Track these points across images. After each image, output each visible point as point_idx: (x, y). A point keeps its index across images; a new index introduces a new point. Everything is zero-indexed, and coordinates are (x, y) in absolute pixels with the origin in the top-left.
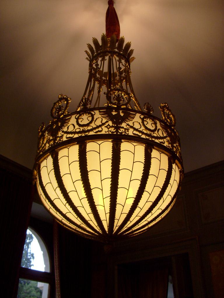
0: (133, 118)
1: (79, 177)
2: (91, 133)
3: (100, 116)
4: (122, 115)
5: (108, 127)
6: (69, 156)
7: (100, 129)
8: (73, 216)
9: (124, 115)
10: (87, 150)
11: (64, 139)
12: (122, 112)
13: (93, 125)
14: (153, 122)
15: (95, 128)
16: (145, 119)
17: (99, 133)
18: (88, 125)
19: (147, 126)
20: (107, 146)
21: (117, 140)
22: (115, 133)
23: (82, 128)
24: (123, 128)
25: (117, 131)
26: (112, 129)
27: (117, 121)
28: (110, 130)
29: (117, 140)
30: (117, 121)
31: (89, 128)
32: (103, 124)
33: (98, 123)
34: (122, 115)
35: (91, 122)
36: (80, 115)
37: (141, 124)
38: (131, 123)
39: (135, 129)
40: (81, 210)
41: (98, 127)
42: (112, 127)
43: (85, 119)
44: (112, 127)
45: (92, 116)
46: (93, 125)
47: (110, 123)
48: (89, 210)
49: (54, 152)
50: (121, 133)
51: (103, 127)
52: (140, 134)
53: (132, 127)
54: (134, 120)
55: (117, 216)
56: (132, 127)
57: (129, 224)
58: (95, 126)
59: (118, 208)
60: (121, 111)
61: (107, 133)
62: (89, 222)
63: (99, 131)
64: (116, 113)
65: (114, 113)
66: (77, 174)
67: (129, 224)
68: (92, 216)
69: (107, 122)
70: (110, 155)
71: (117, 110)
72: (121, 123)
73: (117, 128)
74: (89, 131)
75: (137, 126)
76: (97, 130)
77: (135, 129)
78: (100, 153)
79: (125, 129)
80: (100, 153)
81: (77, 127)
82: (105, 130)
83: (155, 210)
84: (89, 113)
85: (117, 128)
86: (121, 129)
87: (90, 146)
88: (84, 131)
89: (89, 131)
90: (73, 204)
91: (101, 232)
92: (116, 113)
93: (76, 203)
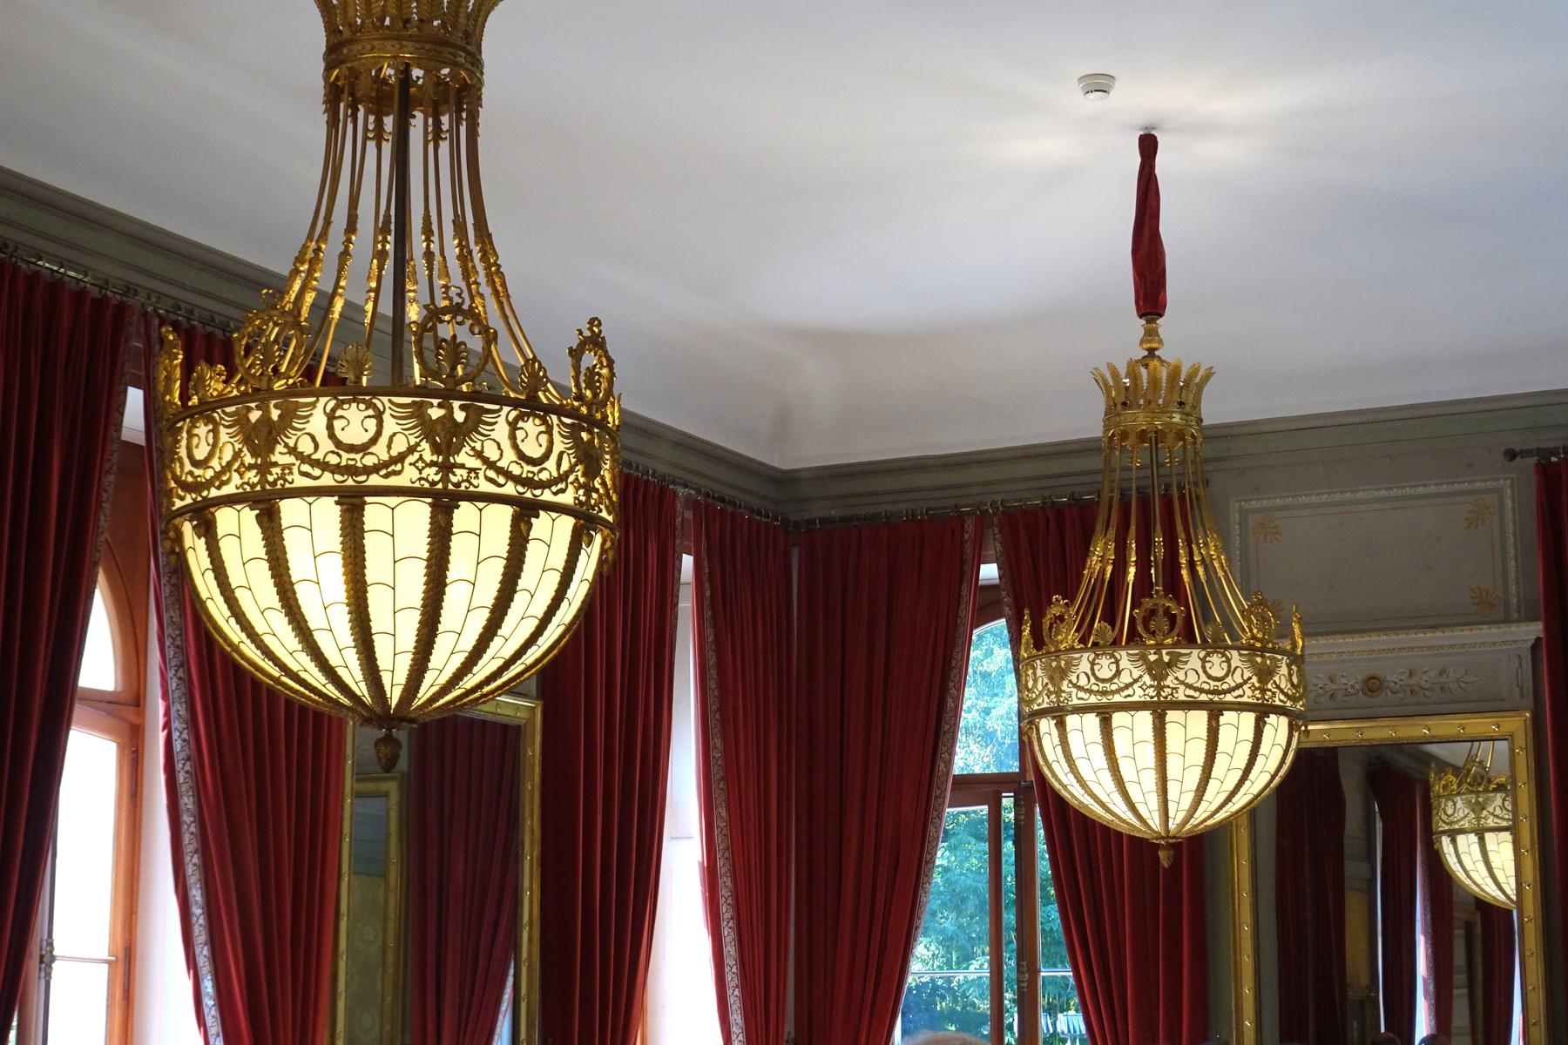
2: (1229, 698)
3: (398, 428)
4: (460, 416)
5: (420, 464)
7: (1130, 691)
8: (316, 677)
9: (466, 419)
11: (1182, 698)
12: (462, 408)
13: (380, 452)
14: (543, 428)
15: (1234, 689)
16: (520, 424)
18: (363, 449)
19: (522, 446)
22: (440, 486)
24: (462, 466)
25: (445, 480)
26: (431, 473)
27: (447, 439)
28: (424, 475)
29: (1262, 712)
30: (447, 439)
31: (1225, 687)
33: (1125, 678)
34: (460, 416)
35: (1227, 675)
36: (1208, 654)
37: (1200, 671)
38: (1181, 676)
39: (1190, 686)
42: (433, 464)
44: (433, 464)
45: (1228, 661)
47: (1147, 679)
49: (1059, 714)
50: (458, 485)
52: (1196, 694)
53: (1182, 683)
56: (1182, 683)
60: (456, 404)
61: (417, 485)
62: (303, 675)
64: (442, 412)
65: (1152, 658)
69: (411, 450)
71: (446, 396)
73: (447, 468)
74: (368, 471)
75: (1192, 679)
76: (1126, 693)
77: (1190, 686)
78: (1134, 729)
79: (471, 470)
81: (1203, 678)
82: (1138, 695)
84: (370, 405)
85: (447, 468)
86: (456, 471)
89: (368, 471)
90: (326, 661)
91: (368, 699)
92: (442, 412)
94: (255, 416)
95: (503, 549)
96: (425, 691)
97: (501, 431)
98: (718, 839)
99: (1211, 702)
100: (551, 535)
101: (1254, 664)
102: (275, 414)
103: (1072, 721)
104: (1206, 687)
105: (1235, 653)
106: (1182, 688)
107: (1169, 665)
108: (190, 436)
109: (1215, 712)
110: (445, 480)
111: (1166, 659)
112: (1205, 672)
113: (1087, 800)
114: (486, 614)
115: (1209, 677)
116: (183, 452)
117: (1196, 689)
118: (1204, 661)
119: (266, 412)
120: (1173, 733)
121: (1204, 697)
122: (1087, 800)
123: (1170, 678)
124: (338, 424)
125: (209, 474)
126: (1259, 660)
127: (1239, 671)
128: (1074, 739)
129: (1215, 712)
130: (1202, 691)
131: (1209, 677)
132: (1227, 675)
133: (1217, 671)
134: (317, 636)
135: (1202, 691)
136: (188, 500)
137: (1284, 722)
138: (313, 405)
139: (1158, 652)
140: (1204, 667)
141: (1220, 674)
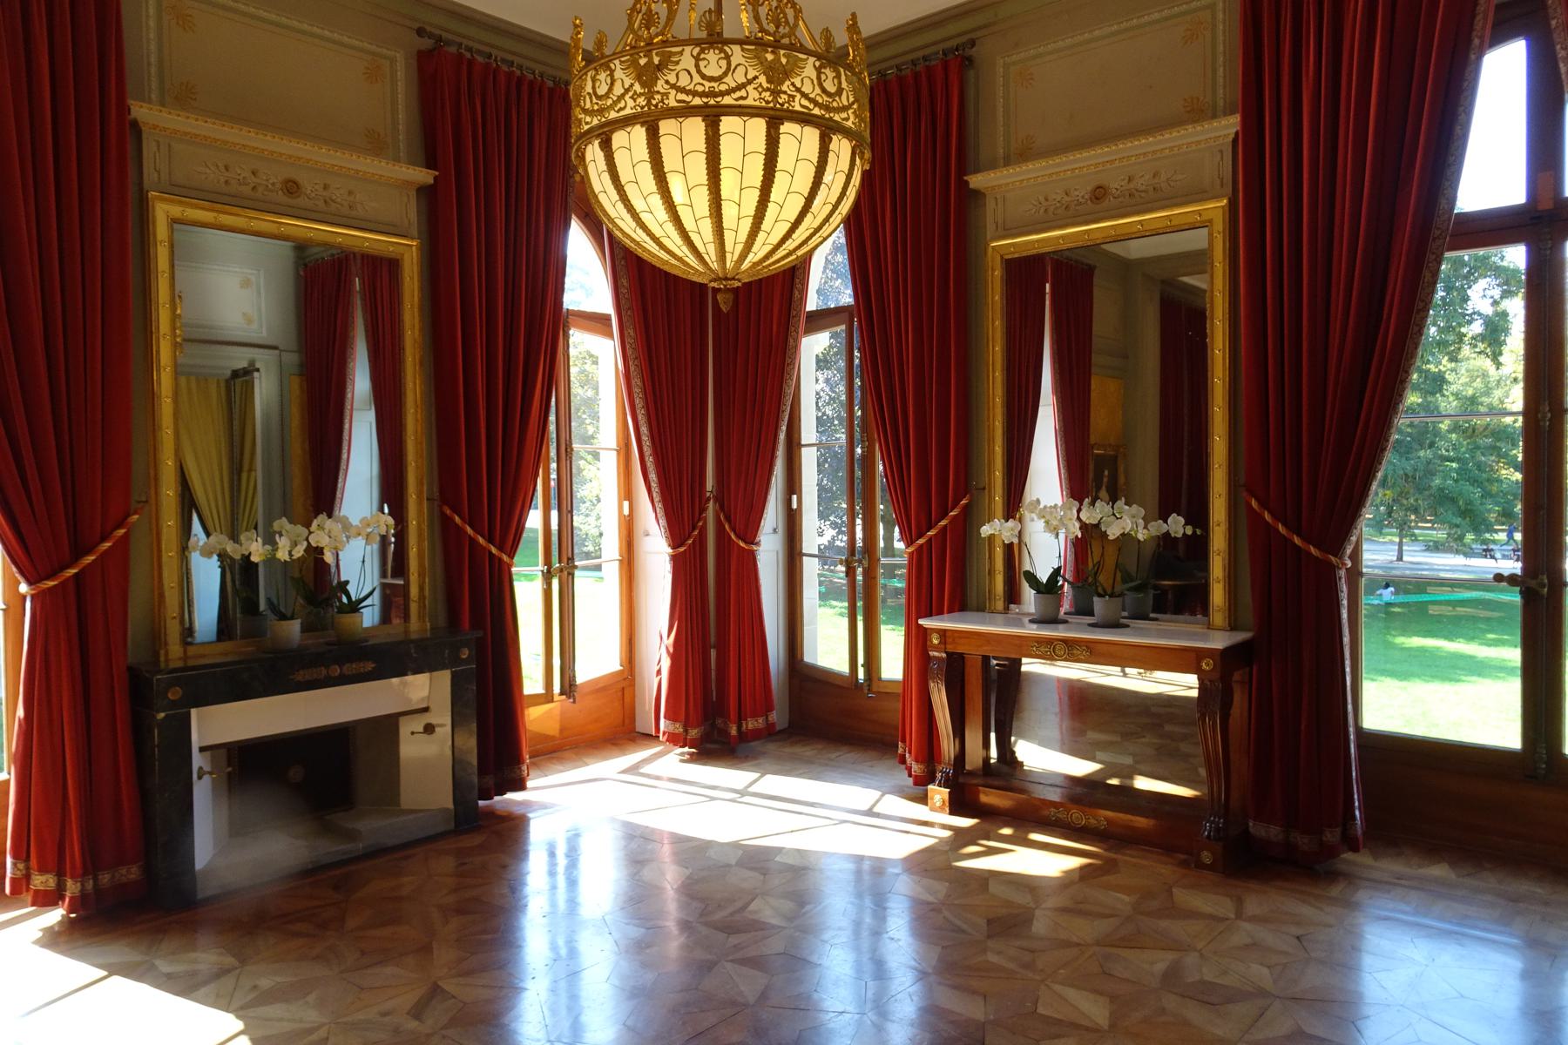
0: (677, 63)
1: (654, 188)
2: (727, 100)
3: (743, 61)
6: (631, 144)
7: (743, 93)
10: (661, 132)
11: (673, 103)
13: (730, 82)
15: (734, 90)
17: (741, 102)
18: (719, 79)
20: (639, 133)
21: (775, 119)
23: (707, 84)
25: (775, 101)
26: (766, 95)
27: (777, 75)
29: (775, 119)
31: (723, 87)
32: (749, 82)
35: (725, 74)
36: (702, 51)
40: (665, 241)
41: (740, 87)
43: (713, 64)
45: (728, 58)
46: (730, 82)
48: (679, 241)
51: (750, 88)
54: (678, 68)
55: (729, 247)
56: (673, 86)
57: (752, 258)
58: (733, 85)
59: (729, 237)
63: (742, 98)
66: (649, 183)
67: (752, 258)
68: (685, 249)
69: (756, 78)
70: (762, 146)
72: (782, 83)
73: (776, 93)
74: (722, 94)
75: (684, 81)
76: (738, 94)
79: (663, 94)
80: (742, 140)
81: (697, 78)
82: (752, 98)
83: (798, 232)
84: (722, 51)
85: (776, 93)
87: (728, 123)
88: (827, 108)
93: (689, 224)
94: (643, 61)
95: (762, 148)
96: (746, 265)
97: (687, 61)
98: (629, 352)
99: (706, 105)
100: (841, 148)
101: (762, 62)
102: (656, 60)
103: (619, 139)
104: (700, 89)
105: (736, 48)
106: (673, 92)
107: (659, 68)
108: (594, 81)
109: (712, 117)
110: (775, 101)
111: (656, 60)
112: (699, 71)
113: (640, 236)
114: (750, 220)
115: (703, 77)
116: (589, 89)
117: (688, 92)
118: (697, 59)
119: (651, 59)
120: (668, 146)
121: (697, 101)
122: (640, 236)
123: (660, 83)
124: (702, 64)
125: (610, 102)
126: (770, 57)
127: (741, 70)
128: (621, 159)
129: (712, 117)
130: (695, 94)
131: (703, 77)
132: (725, 74)
133: (713, 70)
134: (642, 216)
135: (695, 94)
136: (595, 122)
137: (812, 135)
138: (681, 53)
139: (648, 54)
140: (697, 66)
141: (717, 73)
